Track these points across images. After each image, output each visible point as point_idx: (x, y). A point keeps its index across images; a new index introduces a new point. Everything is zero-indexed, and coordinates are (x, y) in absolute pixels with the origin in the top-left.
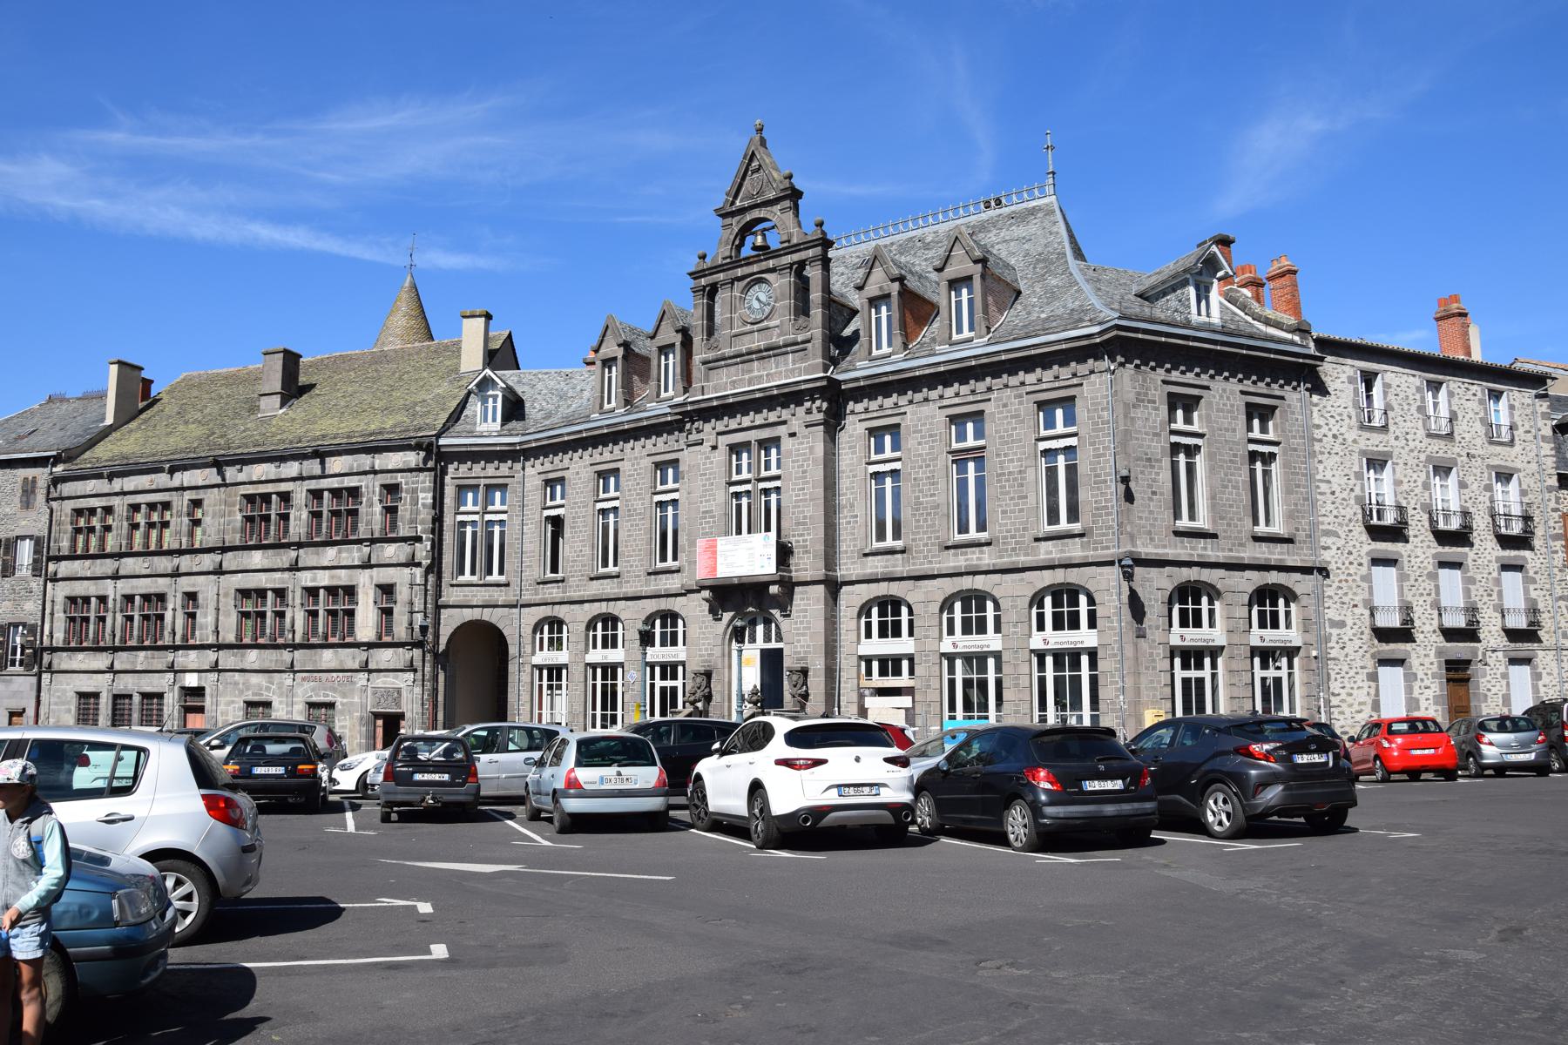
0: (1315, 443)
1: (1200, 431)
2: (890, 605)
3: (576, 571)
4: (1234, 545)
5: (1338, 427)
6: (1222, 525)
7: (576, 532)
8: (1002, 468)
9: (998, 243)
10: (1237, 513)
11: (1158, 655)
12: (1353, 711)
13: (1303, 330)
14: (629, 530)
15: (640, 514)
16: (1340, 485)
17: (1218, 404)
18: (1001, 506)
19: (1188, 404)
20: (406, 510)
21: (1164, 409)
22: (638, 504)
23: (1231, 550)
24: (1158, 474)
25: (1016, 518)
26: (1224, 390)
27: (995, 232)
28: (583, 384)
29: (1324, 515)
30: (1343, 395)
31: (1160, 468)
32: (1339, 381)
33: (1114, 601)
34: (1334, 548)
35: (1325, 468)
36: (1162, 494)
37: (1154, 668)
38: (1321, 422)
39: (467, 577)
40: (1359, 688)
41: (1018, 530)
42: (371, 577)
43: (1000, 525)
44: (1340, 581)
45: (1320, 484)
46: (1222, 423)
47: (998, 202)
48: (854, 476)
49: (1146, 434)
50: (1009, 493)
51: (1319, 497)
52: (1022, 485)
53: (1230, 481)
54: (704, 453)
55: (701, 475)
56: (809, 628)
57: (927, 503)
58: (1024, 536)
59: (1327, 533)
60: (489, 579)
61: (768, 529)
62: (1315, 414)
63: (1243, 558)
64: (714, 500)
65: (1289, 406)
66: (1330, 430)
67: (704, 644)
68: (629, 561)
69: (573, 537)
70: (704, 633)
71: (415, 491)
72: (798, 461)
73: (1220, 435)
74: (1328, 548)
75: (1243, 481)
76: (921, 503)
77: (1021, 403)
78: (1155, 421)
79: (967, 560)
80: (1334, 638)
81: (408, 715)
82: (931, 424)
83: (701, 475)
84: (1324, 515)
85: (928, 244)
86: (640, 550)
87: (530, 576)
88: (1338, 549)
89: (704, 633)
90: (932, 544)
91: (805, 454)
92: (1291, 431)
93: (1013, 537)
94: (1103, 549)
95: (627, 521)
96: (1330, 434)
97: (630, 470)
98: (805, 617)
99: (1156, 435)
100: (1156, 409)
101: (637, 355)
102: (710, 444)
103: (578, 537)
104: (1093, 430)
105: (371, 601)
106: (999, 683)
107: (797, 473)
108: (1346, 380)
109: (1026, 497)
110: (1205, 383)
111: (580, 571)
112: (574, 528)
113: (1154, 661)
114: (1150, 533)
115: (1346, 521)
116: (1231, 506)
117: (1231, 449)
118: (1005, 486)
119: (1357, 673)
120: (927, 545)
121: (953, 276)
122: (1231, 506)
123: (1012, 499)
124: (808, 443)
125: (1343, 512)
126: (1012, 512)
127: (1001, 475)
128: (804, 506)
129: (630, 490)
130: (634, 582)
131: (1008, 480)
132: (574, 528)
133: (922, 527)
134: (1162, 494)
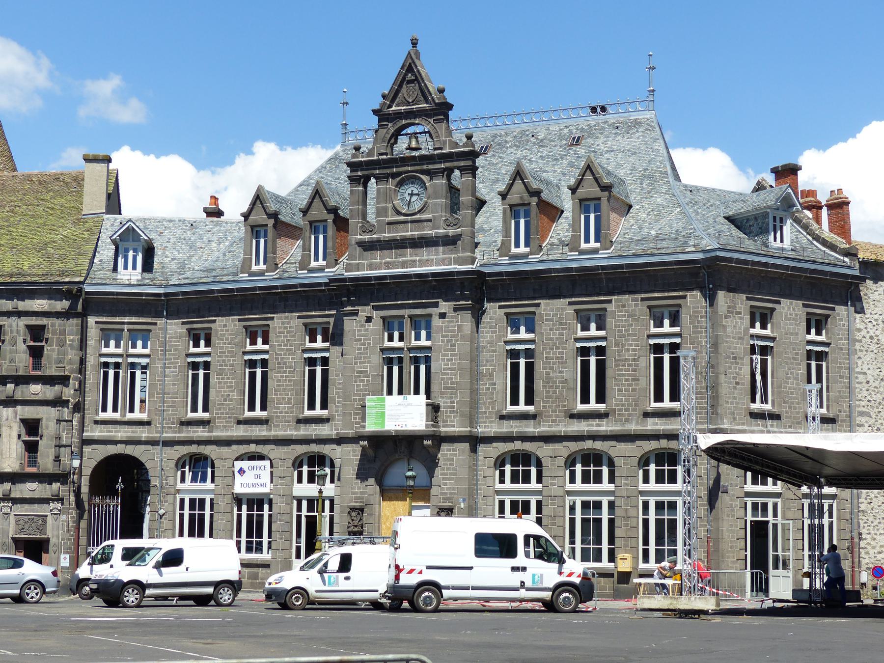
0: (857, 343)
1: (772, 335)
2: (521, 459)
3: (223, 413)
4: (793, 423)
5: (874, 330)
6: (785, 407)
7: (223, 379)
8: (619, 355)
9: (607, 152)
10: (795, 398)
11: (736, 505)
12: (876, 552)
13: (851, 253)
14: (279, 381)
15: (290, 367)
16: (873, 376)
18: (618, 385)
19: (763, 317)
20: (53, 350)
21: (747, 318)
22: (288, 359)
24: (740, 369)
27: (602, 139)
28: (209, 235)
29: (860, 400)
31: (743, 364)
32: (876, 293)
34: (867, 425)
36: (743, 384)
37: (733, 516)
39: (109, 415)
40: (880, 534)
42: (16, 413)
45: (859, 376)
47: (603, 109)
48: (494, 351)
49: (734, 338)
50: (624, 375)
51: (857, 385)
52: (635, 370)
53: (792, 374)
54: (360, 322)
55: (356, 340)
56: (455, 474)
57: (556, 378)
58: (635, 410)
59: (862, 414)
60: (130, 416)
61: (417, 392)
62: (858, 321)
64: (369, 362)
65: (838, 315)
66: (868, 332)
68: (278, 408)
69: (220, 383)
71: (63, 333)
72: (447, 336)
73: (786, 339)
74: (863, 425)
75: (802, 374)
76: (552, 378)
77: (636, 305)
78: (740, 328)
79: (588, 425)
81: (53, 541)
82: (562, 314)
84: (860, 400)
85: (542, 140)
88: (870, 426)
92: (838, 334)
93: (626, 410)
96: (868, 336)
98: (451, 464)
99: (740, 338)
100: (742, 319)
101: (283, 223)
102: (366, 314)
105: (15, 435)
106: (611, 522)
108: (882, 293)
111: (227, 413)
112: (221, 374)
113: (733, 510)
114: (733, 414)
115: (877, 404)
116: (792, 393)
117: (794, 349)
119: (880, 523)
121: (584, 197)
122: (792, 393)
123: (627, 380)
124: (457, 322)
125: (875, 397)
127: (618, 360)
130: (283, 426)
131: (624, 365)
133: (551, 397)
134: (743, 384)
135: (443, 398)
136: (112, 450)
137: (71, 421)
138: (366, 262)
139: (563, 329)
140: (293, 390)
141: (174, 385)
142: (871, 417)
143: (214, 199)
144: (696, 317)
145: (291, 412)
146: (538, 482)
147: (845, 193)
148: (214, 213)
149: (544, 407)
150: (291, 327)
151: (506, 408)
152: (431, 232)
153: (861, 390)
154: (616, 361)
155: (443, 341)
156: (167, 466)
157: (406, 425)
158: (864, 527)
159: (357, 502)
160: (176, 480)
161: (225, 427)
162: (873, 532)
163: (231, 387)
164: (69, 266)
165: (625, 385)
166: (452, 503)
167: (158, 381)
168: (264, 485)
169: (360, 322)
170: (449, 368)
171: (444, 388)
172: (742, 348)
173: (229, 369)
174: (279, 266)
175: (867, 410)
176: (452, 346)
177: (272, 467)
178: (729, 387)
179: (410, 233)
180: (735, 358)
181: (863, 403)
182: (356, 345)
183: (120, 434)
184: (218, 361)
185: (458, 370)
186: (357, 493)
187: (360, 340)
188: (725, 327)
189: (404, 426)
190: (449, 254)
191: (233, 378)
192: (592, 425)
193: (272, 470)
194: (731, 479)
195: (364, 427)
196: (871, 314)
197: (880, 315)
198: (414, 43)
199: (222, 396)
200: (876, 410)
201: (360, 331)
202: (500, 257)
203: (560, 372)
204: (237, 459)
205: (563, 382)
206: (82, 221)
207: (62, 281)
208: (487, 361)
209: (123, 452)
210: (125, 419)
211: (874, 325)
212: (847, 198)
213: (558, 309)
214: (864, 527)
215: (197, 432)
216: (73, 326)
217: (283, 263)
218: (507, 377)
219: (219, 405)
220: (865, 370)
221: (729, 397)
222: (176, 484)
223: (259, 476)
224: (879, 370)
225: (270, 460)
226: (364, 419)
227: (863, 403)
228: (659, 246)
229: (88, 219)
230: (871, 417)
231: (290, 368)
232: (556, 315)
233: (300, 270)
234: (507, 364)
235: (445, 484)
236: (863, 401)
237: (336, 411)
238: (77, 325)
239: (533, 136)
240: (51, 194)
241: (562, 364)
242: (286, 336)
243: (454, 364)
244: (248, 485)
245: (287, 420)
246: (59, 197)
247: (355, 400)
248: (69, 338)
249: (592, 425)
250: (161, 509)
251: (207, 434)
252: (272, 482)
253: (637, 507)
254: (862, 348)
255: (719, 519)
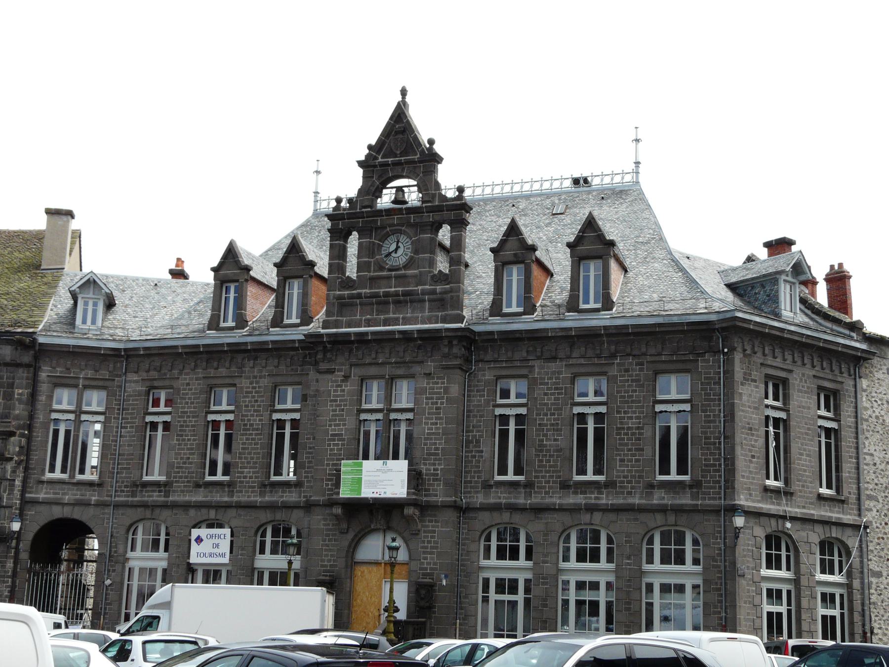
3: (181, 477)
6: (798, 486)
14: (244, 444)
15: (257, 429)
17: (799, 385)
18: (620, 455)
22: (255, 420)
23: (804, 507)
25: (632, 466)
26: (803, 375)
29: (868, 483)
30: (883, 384)
32: (881, 372)
33: (719, 543)
34: (875, 510)
35: (870, 443)
38: (868, 405)
41: (634, 477)
43: (618, 471)
44: (878, 538)
45: (866, 457)
46: (801, 402)
49: (749, 407)
50: (627, 444)
51: (865, 467)
52: (639, 439)
54: (336, 381)
55: (331, 401)
56: (436, 548)
57: (550, 445)
59: (870, 497)
63: (813, 515)
64: (344, 425)
67: (326, 555)
68: (242, 473)
69: (179, 445)
70: (327, 545)
72: (432, 398)
73: (799, 412)
74: (871, 510)
76: (546, 446)
77: (641, 370)
79: (586, 498)
80: (874, 586)
83: (331, 401)
84: (868, 483)
86: (255, 463)
87: (125, 477)
89: (327, 545)
90: (554, 482)
91: (439, 393)
94: (710, 499)
95: (243, 435)
97: (249, 388)
98: (432, 537)
99: (755, 408)
100: (757, 387)
103: (186, 445)
104: (706, 400)
107: (430, 408)
108: (886, 372)
109: (642, 450)
110: (790, 367)
111: (186, 477)
112: (182, 435)
114: (749, 489)
115: (883, 489)
116: (805, 471)
118: (623, 439)
120: (548, 482)
124: (443, 383)
126: (629, 461)
128: (436, 439)
129: (247, 406)
131: (627, 434)
132: (182, 435)
133: (545, 466)
135: (425, 464)
136: (57, 512)
137: (14, 480)
138: (345, 319)
139: (558, 394)
140: (259, 453)
141: (129, 445)
142: (878, 502)
143: (179, 260)
144: (709, 384)
145: (256, 477)
146: (527, 559)
147: (846, 267)
148: (178, 274)
149: (536, 477)
150: (259, 387)
151: (493, 478)
152: (416, 288)
153: (869, 472)
154: (618, 429)
155: (427, 404)
156: (118, 533)
157: (385, 493)
158: (875, 621)
159: (326, 576)
160: (126, 547)
161: (183, 491)
162: (884, 627)
163: (192, 449)
164: (23, 317)
165: (627, 455)
166: (433, 579)
167: (112, 441)
168: (223, 555)
169: (336, 381)
170: (434, 433)
171: (427, 454)
172: (756, 419)
173: (190, 430)
174: (249, 323)
175: (875, 494)
176: (437, 409)
177: (232, 535)
178: (745, 460)
179: (393, 289)
180: (750, 429)
181: (871, 486)
182: (332, 406)
183: (67, 497)
184: (179, 422)
185: (443, 434)
186: (326, 566)
187: (336, 401)
188: (741, 394)
189: (382, 493)
190: (436, 312)
191: (194, 440)
192: (591, 498)
193: (232, 539)
194: (748, 561)
195: (338, 493)
196: (876, 392)
197: (885, 394)
198: (404, 92)
199: (182, 458)
200: (883, 495)
201: (335, 391)
202: (490, 316)
203: (555, 440)
204: (194, 527)
205: (558, 451)
206: (40, 275)
207: (14, 331)
208: (473, 427)
209: (69, 516)
210: (75, 481)
211: (879, 405)
212: (848, 272)
213: (554, 373)
214: (875, 620)
215: (152, 496)
216: (22, 379)
217: (254, 320)
218: (494, 444)
219: (177, 468)
220: (872, 451)
221: (745, 471)
222: (126, 552)
223: (217, 546)
224: (885, 452)
225: (231, 528)
226: (337, 485)
227: (871, 486)
228: (666, 308)
229: (47, 273)
230: (878, 502)
231: (257, 431)
232: (551, 378)
233: (272, 327)
234: (495, 431)
235: (426, 558)
236: (870, 483)
237: (306, 477)
238: (27, 378)
239: (513, 206)
240: (9, 249)
241: (557, 431)
242: (254, 397)
243: (437, 429)
244: (204, 555)
245: (251, 486)
246: (17, 252)
247: (328, 465)
248: (17, 391)
249: (591, 498)
250: (107, 579)
251: (163, 499)
252: (231, 552)
253: (640, 589)
254: (868, 428)
255: (736, 605)
